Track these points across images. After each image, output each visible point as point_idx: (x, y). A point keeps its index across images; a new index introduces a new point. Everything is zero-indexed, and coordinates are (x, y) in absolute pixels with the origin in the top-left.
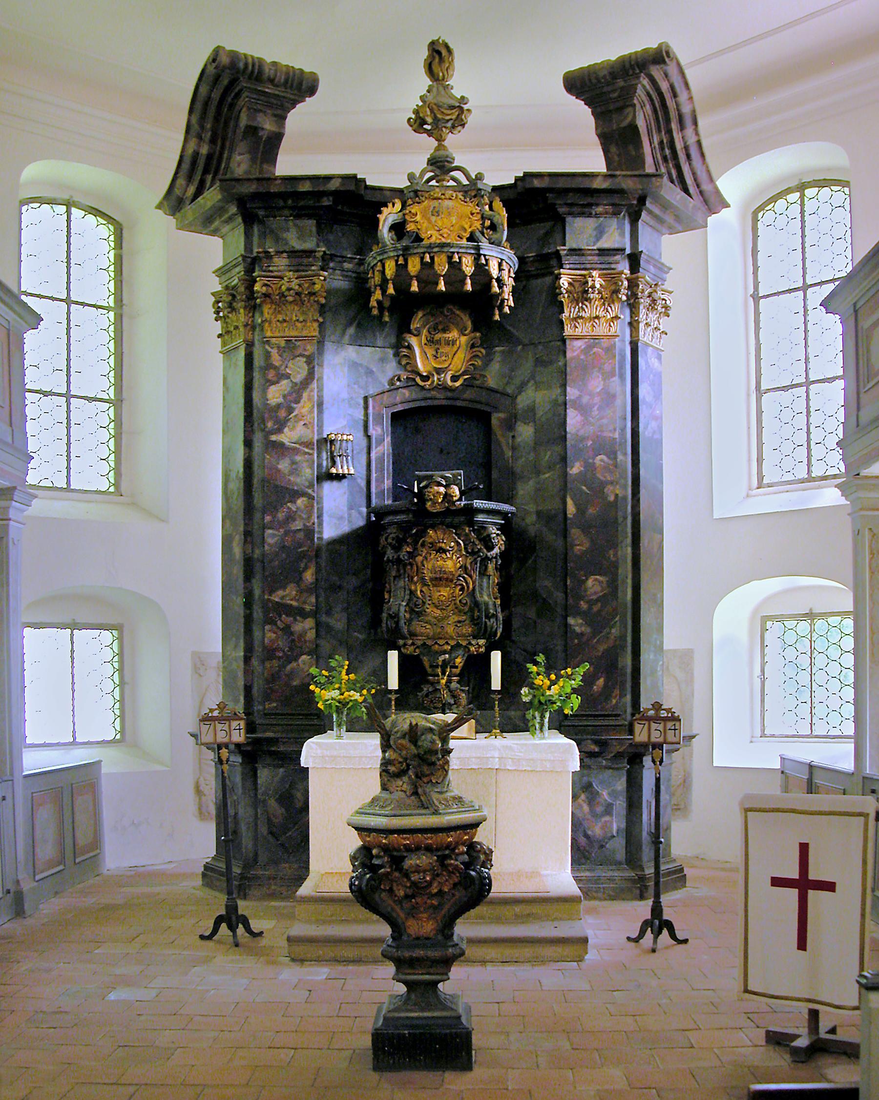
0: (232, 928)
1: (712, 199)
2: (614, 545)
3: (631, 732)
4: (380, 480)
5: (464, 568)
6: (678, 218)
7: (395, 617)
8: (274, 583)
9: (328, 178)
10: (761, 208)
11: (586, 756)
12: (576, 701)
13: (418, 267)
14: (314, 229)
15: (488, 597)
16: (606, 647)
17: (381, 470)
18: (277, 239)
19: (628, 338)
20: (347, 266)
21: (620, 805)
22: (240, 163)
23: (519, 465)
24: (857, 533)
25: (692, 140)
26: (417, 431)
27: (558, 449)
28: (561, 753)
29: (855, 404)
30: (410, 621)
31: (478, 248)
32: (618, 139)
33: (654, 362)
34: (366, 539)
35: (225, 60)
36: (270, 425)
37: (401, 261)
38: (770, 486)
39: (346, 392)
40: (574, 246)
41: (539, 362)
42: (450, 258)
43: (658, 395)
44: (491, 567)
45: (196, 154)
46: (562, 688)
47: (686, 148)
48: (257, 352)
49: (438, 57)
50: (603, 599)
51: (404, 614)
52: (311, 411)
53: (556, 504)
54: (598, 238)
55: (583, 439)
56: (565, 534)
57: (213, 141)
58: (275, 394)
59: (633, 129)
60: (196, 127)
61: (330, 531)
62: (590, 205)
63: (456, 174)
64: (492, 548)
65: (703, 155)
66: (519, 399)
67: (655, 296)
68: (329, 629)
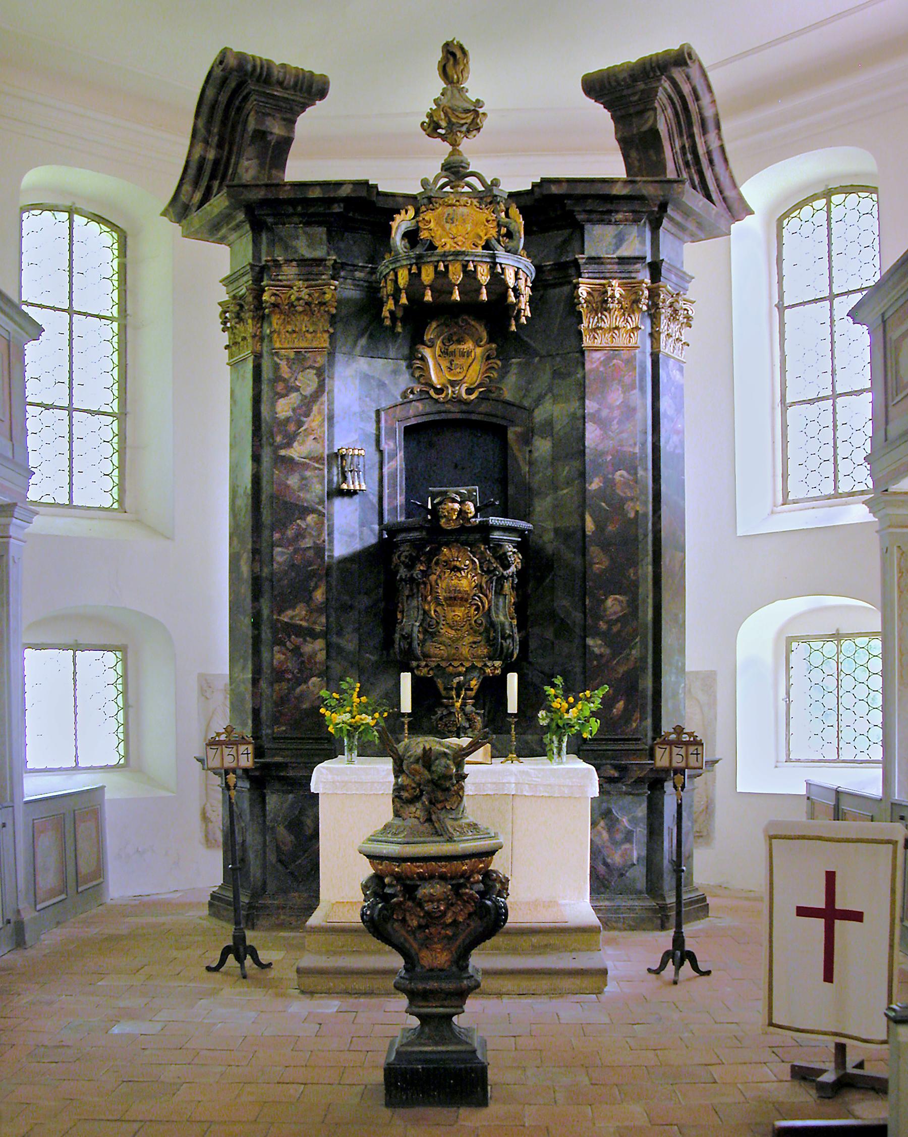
0: (240, 959)
1: (736, 206)
2: (634, 563)
3: (652, 756)
4: (393, 497)
5: (479, 587)
6: (700, 226)
7: (408, 637)
8: (283, 603)
9: (339, 184)
10: (786, 215)
11: (606, 781)
12: (595, 725)
13: (432, 276)
14: (324, 237)
15: (504, 617)
16: (626, 669)
17: (393, 486)
18: (286, 247)
19: (648, 350)
20: (358, 274)
21: (641, 832)
22: (248, 169)
23: (536, 481)
24: (886, 551)
25: (714, 145)
26: (431, 445)
27: (576, 464)
28: (579, 778)
29: (883, 417)
30: (423, 642)
31: (494, 257)
32: (638, 144)
33: (676, 374)
34: (379, 557)
35: (232, 62)
36: (279, 439)
37: (414, 270)
38: (795, 502)
39: (358, 405)
40: (593, 254)
41: (556, 374)
42: (465, 267)
43: (680, 409)
44: (507, 586)
45: (203, 159)
46: (581, 711)
47: (709, 153)
48: (266, 364)
49: (453, 59)
50: (623, 620)
51: (417, 635)
52: (321, 425)
53: (575, 521)
54: (618, 246)
55: (603, 454)
56: (584, 552)
57: (220, 146)
58: (284, 408)
59: (654, 133)
60: (202, 131)
61: (341, 549)
62: (610, 212)
63: (471, 180)
64: (508, 567)
65: (726, 160)
66: (536, 412)
67: (677, 306)
68: (340, 650)
